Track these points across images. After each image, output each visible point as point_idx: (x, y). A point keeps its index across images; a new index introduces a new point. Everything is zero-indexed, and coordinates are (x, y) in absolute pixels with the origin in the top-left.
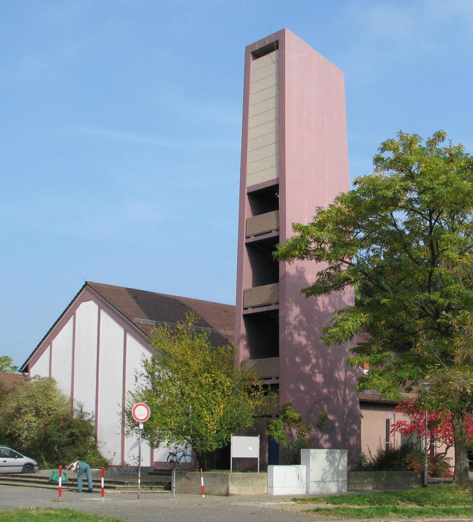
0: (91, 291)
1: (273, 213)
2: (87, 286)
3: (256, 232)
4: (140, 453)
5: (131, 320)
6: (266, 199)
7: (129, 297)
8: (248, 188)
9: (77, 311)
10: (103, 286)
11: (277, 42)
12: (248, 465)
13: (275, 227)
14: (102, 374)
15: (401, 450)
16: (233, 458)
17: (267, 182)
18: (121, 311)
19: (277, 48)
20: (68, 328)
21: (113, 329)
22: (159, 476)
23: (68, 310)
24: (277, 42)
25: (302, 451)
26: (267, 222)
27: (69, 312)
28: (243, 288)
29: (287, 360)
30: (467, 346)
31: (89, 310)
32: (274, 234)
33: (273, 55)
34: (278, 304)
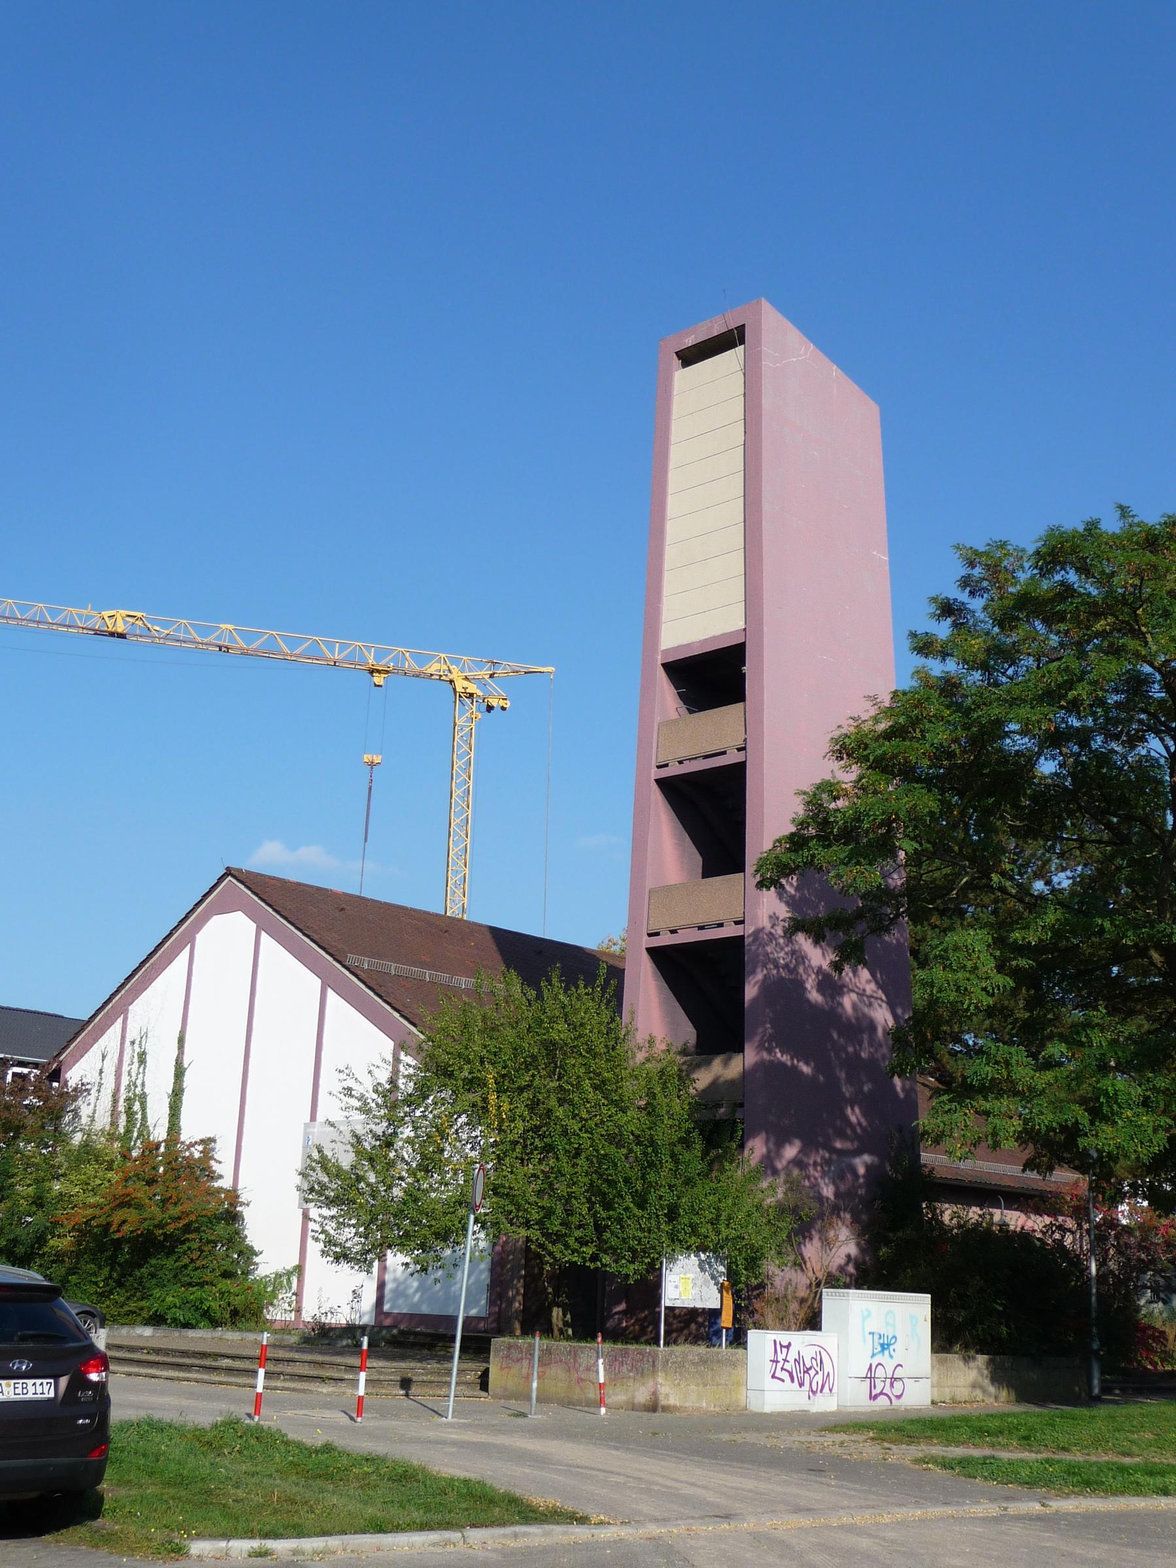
0: (229, 872)
2: (230, 878)
4: (338, 1293)
6: (712, 677)
8: (666, 652)
9: (198, 936)
11: (741, 329)
12: (694, 1325)
14: (255, 1075)
15: (80, 1195)
16: (666, 1308)
17: (714, 638)
18: (316, 937)
19: (742, 342)
20: (173, 974)
21: (291, 980)
22: (406, 1339)
24: (741, 329)
26: (710, 735)
27: (177, 937)
28: (649, 884)
30: (1173, 1063)
31: (230, 934)
33: (731, 359)
34: (742, 922)
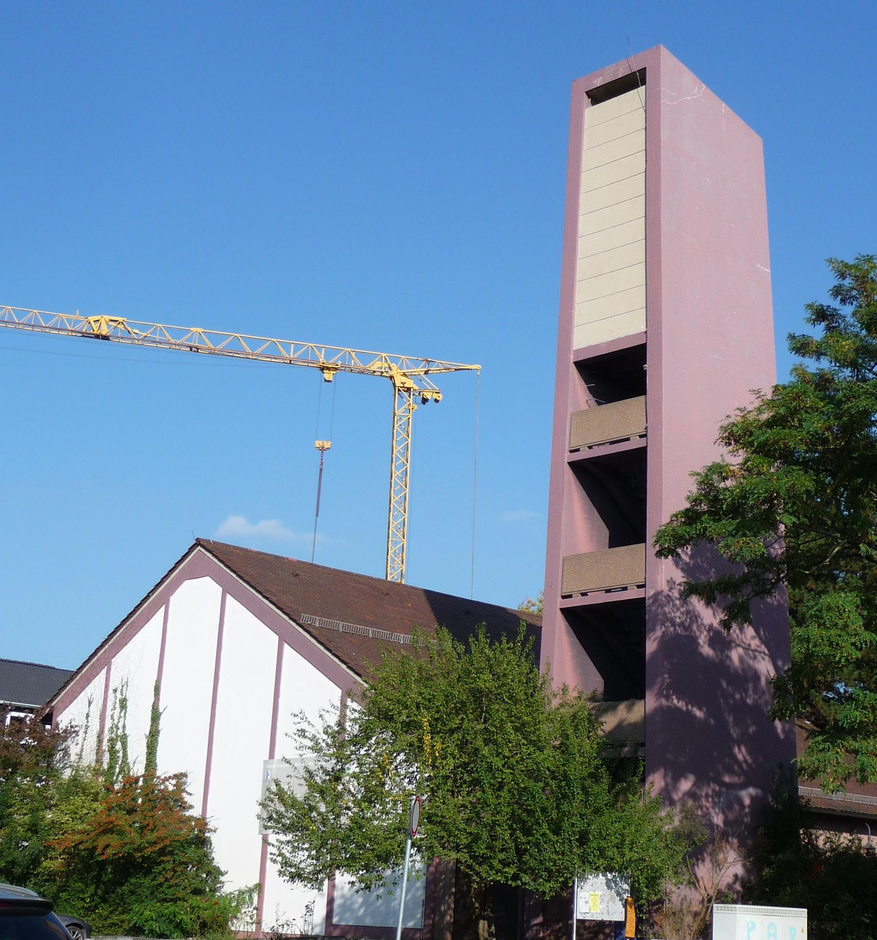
0: (199, 543)
1: (643, 397)
2: (199, 548)
3: (591, 440)
5: (296, 618)
6: (618, 374)
7: (424, 598)
9: (171, 598)
10: (232, 550)
11: (643, 72)
13: (642, 431)
18: (274, 599)
20: (148, 635)
23: (139, 612)
24: (643, 72)
25: (715, 909)
28: (563, 553)
29: (699, 713)
32: (635, 443)
33: (634, 98)
34: (644, 586)
